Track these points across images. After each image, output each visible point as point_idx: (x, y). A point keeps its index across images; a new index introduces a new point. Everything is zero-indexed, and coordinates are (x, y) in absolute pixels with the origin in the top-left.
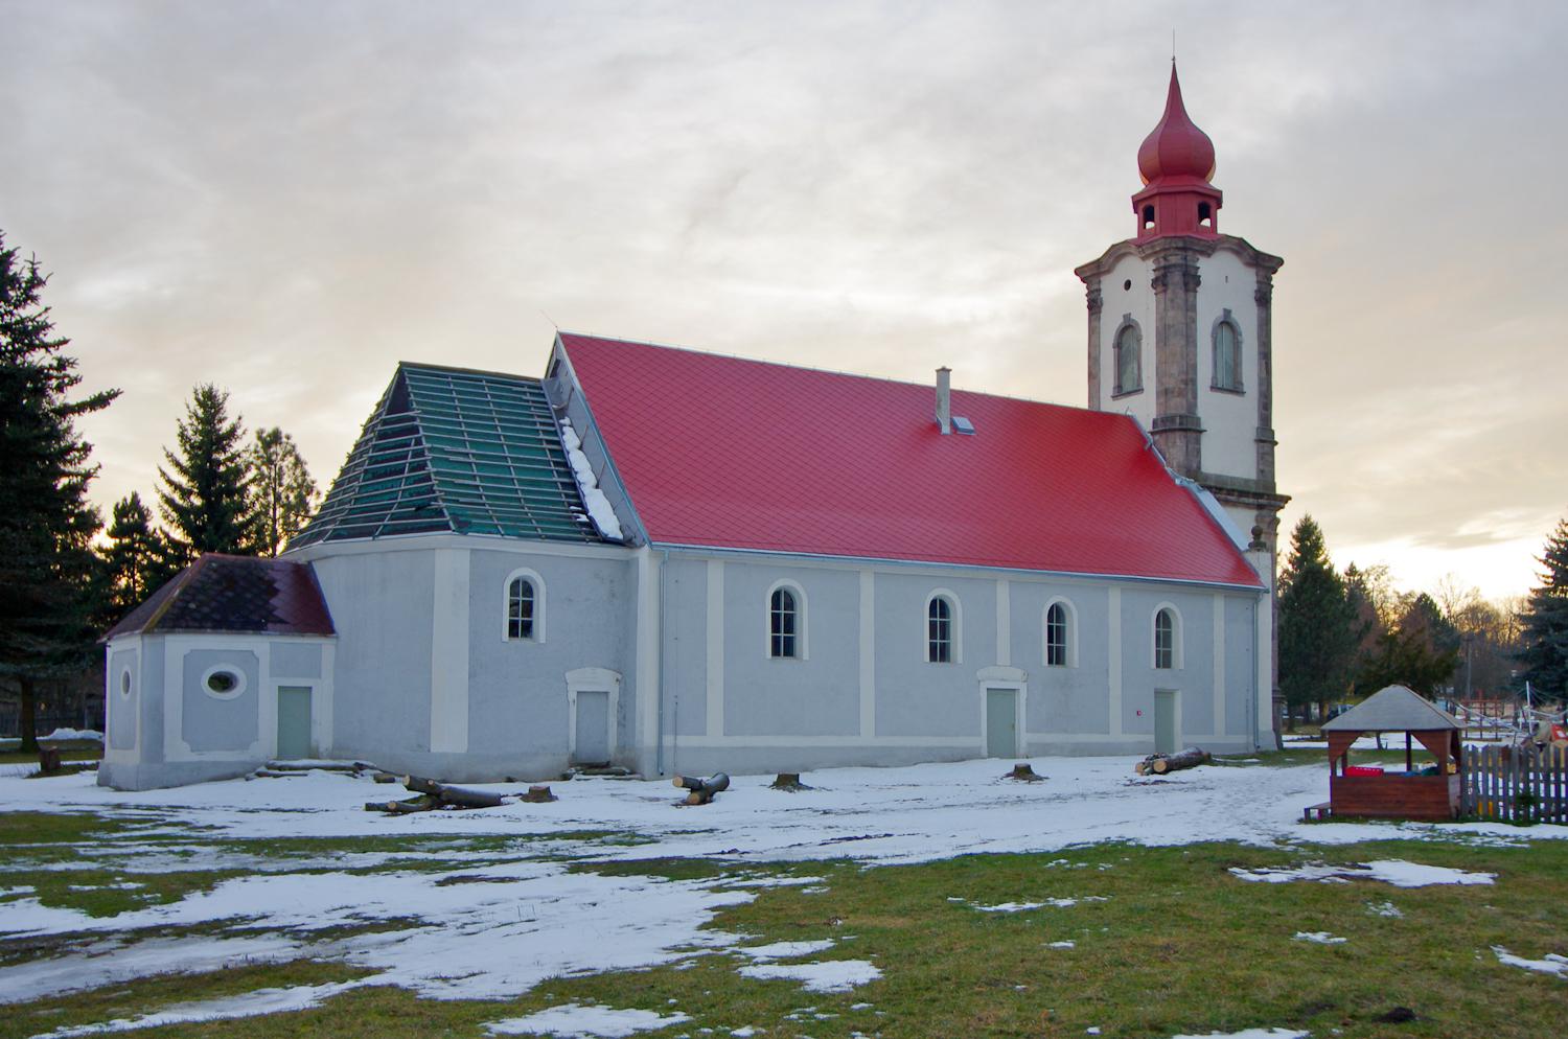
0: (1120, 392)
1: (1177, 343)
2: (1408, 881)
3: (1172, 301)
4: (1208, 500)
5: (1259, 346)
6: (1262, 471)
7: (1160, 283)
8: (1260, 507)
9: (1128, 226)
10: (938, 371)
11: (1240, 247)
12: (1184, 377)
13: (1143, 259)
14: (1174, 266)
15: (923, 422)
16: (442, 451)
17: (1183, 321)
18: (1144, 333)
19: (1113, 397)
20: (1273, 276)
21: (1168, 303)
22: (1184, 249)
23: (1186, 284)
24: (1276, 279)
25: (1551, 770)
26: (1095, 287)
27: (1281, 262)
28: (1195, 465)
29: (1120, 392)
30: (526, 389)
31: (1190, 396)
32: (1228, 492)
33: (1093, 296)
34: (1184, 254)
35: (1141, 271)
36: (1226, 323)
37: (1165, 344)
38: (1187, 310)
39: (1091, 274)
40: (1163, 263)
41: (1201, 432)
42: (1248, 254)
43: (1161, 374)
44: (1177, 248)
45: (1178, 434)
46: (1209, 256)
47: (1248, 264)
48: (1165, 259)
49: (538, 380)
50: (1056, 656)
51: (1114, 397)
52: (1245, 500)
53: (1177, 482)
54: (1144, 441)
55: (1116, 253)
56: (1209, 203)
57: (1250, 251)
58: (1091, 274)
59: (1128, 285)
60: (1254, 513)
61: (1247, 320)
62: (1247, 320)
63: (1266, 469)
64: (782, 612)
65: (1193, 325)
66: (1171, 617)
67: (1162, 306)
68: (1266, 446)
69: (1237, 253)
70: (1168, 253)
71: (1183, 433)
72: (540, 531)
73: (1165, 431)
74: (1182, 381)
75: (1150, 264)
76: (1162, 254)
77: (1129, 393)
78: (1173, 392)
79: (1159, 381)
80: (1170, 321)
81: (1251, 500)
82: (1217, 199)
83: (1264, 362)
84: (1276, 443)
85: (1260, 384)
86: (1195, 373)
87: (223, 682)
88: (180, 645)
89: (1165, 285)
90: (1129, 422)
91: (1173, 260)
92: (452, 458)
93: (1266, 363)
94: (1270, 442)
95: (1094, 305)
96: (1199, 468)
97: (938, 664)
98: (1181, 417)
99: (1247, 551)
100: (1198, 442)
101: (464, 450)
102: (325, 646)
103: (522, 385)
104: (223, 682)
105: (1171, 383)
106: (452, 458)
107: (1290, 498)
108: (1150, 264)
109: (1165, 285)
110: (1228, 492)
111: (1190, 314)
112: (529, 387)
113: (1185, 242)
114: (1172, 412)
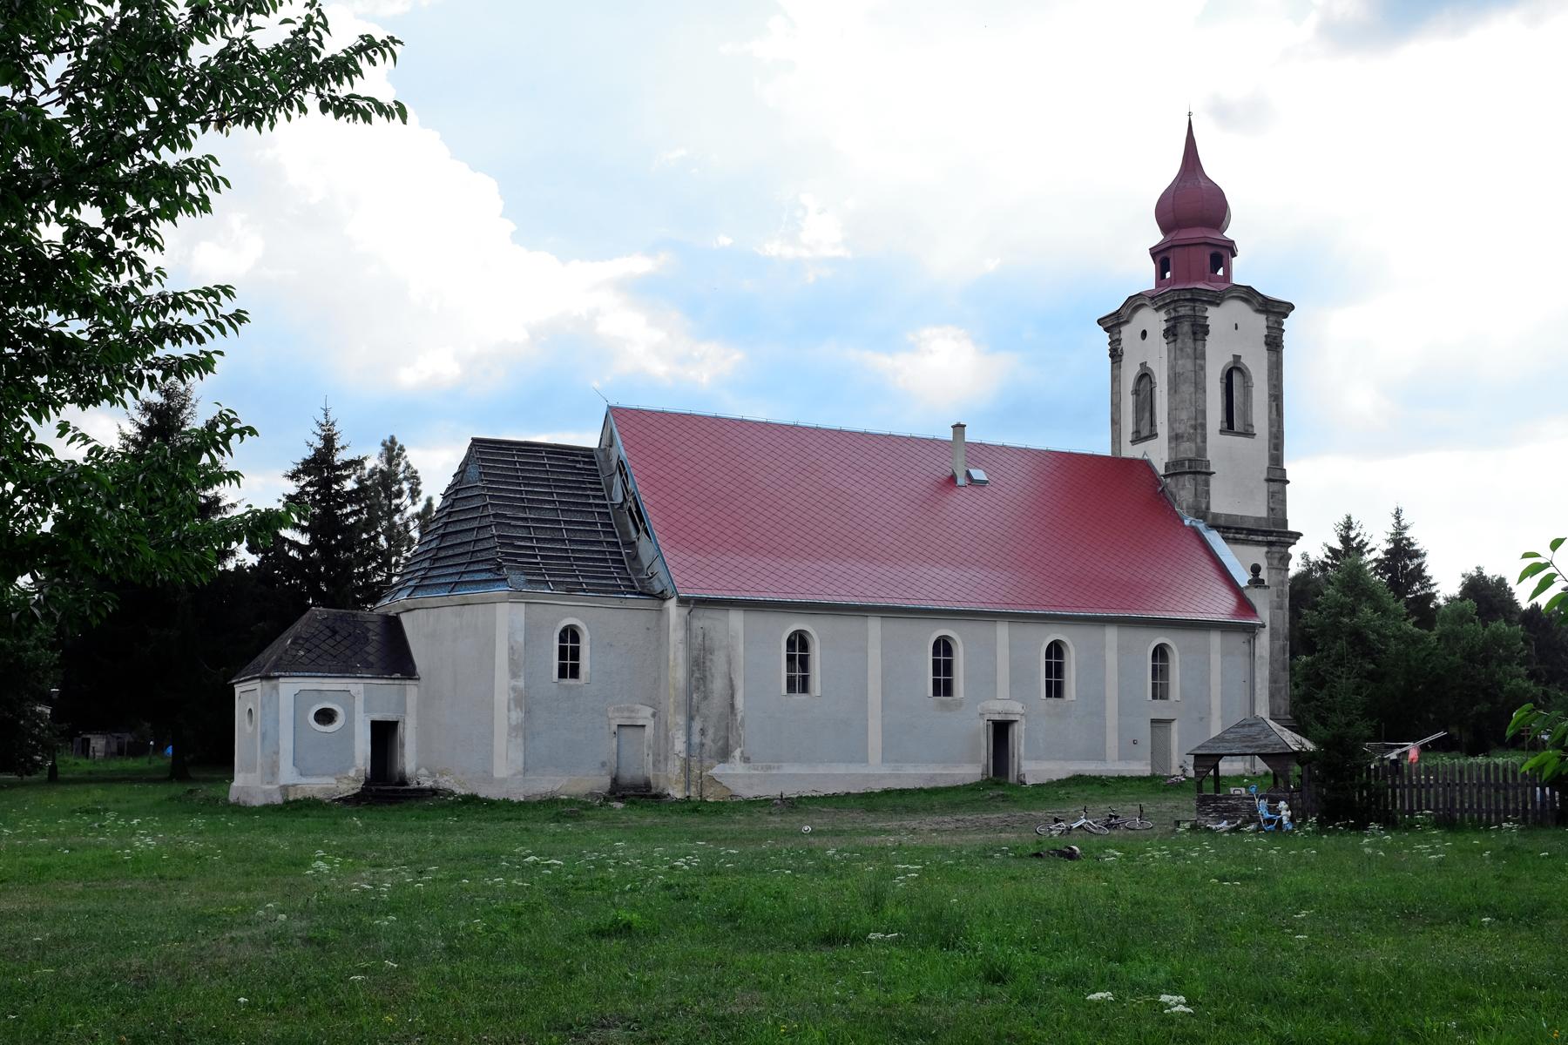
0: (1138, 438)
1: (1187, 389)
2: (366, 759)
4: (1215, 539)
6: (1273, 509)
7: (1171, 333)
8: (1270, 544)
9: (1144, 277)
11: (1248, 295)
12: (1193, 422)
13: (1157, 310)
14: (1184, 316)
15: (939, 475)
16: (505, 516)
21: (1178, 352)
22: (1192, 300)
23: (1194, 333)
26: (1116, 337)
27: (1291, 307)
28: (1204, 506)
29: (1138, 438)
30: (580, 458)
31: (1199, 440)
32: (1236, 532)
35: (1153, 321)
36: (1234, 373)
38: (1196, 358)
39: (1113, 323)
40: (1173, 315)
42: (1258, 302)
43: (1172, 421)
45: (1187, 477)
47: (1257, 311)
49: (591, 450)
50: (1055, 689)
51: (1133, 442)
53: (1187, 522)
54: (1159, 483)
55: (1134, 304)
56: (1223, 253)
57: (1260, 299)
58: (1113, 323)
59: (1144, 334)
60: (1265, 549)
64: (797, 653)
65: (1202, 373)
66: (1064, 648)
67: (1172, 356)
68: (1276, 486)
72: (585, 586)
74: (1191, 426)
75: (1162, 315)
77: (1146, 438)
78: (1182, 437)
81: (1260, 538)
82: (1230, 248)
83: (1274, 404)
84: (1288, 482)
85: (1271, 426)
86: (1204, 418)
87: (325, 716)
88: (289, 687)
89: (1175, 335)
90: (1145, 465)
91: (1183, 311)
92: (513, 523)
93: (1277, 405)
94: (1280, 481)
95: (1116, 355)
96: (1208, 508)
97: (1052, 700)
98: (1190, 460)
99: (1247, 587)
100: (1207, 484)
101: (525, 516)
102: (412, 690)
103: (577, 455)
104: (325, 716)
106: (513, 523)
108: (1162, 315)
109: (1175, 335)
110: (1236, 532)
111: (1198, 362)
112: (547, 452)
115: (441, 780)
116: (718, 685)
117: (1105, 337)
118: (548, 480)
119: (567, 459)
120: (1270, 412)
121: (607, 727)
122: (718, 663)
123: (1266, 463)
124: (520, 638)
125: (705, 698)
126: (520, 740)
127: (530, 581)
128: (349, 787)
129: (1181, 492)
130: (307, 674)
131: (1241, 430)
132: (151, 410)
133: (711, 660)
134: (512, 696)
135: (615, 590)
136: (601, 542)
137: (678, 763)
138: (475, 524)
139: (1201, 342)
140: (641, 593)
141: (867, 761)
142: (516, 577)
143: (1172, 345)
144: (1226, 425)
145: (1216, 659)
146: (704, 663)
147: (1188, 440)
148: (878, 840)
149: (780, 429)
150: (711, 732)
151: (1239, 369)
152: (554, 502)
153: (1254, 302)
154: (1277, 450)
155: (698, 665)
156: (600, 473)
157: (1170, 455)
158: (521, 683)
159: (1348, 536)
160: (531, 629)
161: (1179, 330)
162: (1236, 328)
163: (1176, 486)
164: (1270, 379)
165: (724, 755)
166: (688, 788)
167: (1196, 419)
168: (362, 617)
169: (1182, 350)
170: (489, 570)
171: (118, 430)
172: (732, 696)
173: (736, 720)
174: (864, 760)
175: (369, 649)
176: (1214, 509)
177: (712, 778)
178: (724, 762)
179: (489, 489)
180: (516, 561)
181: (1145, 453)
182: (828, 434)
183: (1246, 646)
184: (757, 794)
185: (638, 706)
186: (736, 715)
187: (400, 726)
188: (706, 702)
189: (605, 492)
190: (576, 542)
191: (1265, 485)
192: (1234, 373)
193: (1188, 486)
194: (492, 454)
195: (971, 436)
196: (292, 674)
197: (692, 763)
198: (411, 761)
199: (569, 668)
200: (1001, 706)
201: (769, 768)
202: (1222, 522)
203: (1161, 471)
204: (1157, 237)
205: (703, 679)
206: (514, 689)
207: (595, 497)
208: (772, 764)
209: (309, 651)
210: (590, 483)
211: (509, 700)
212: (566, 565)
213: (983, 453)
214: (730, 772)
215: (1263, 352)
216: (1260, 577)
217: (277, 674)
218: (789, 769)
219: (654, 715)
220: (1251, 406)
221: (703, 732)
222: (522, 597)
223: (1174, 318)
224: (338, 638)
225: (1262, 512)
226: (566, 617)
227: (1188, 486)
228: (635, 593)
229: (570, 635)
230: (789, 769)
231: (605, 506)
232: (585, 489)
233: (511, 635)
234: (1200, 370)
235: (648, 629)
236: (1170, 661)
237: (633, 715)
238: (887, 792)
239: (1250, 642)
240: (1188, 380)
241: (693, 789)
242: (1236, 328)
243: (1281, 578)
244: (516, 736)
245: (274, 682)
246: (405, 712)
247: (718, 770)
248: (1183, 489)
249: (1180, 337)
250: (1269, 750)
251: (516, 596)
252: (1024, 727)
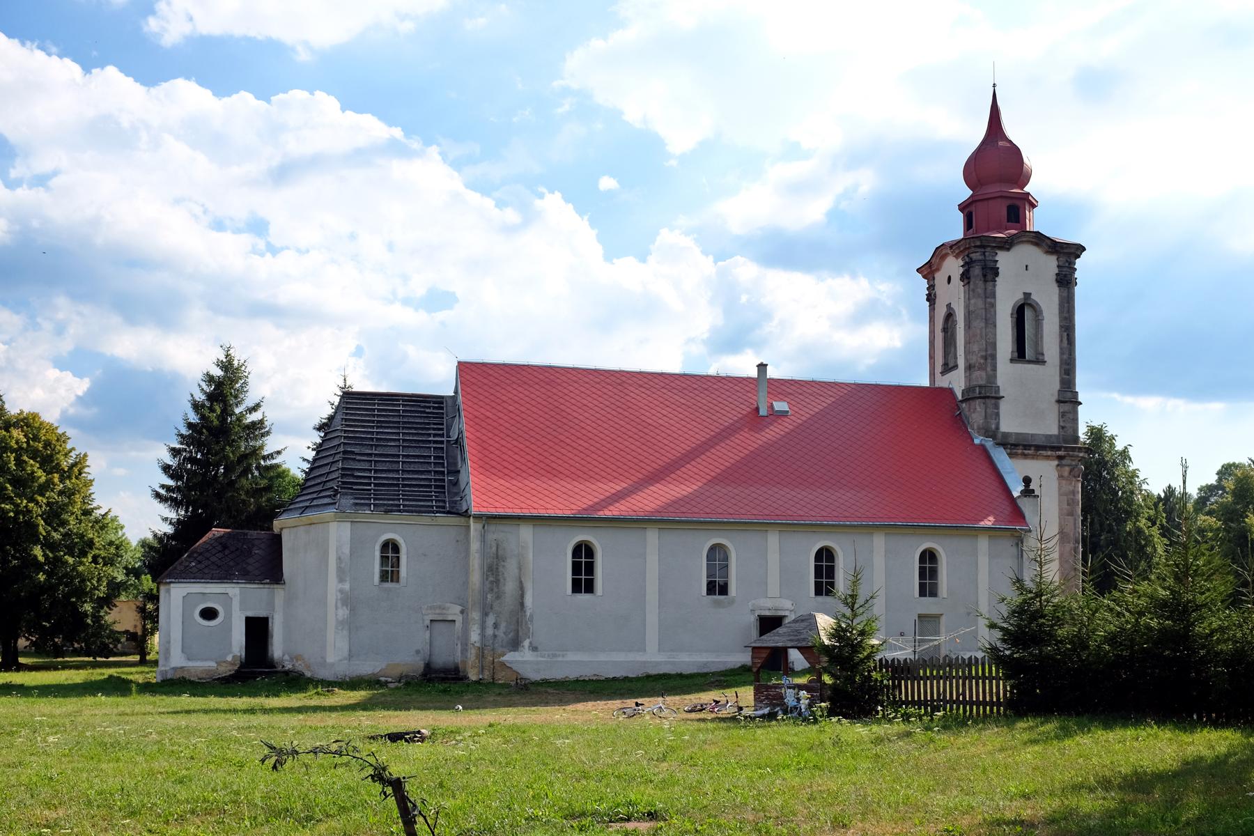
1: (978, 324)
5: (1060, 321)
6: (1063, 428)
10: (758, 366)
11: (1039, 240)
12: (984, 354)
16: (353, 453)
17: (983, 306)
23: (985, 276)
25: (980, 678)
26: (932, 283)
28: (993, 426)
30: (432, 405)
31: (989, 369)
34: (983, 250)
37: (969, 327)
39: (928, 271)
42: (1047, 244)
43: (967, 352)
44: (975, 247)
45: (978, 401)
46: (1008, 249)
47: (1047, 252)
48: (968, 256)
51: (943, 373)
52: (1044, 453)
53: (977, 441)
57: (1049, 242)
60: (1056, 463)
61: (1048, 300)
62: (1048, 300)
63: (1068, 425)
65: (992, 310)
68: (1066, 407)
69: (1037, 244)
70: (971, 251)
71: (983, 401)
74: (982, 357)
76: (966, 253)
78: (974, 367)
79: (966, 359)
81: (1049, 453)
83: (1065, 334)
84: (1081, 403)
85: (1062, 353)
87: (209, 614)
90: (950, 391)
93: (1068, 335)
95: (931, 298)
96: (998, 428)
98: (980, 387)
99: (1019, 497)
100: (997, 407)
101: (370, 452)
102: (279, 593)
103: (429, 402)
104: (209, 614)
109: (969, 278)
111: (988, 300)
112: (434, 403)
113: (981, 241)
115: (297, 664)
116: (510, 587)
117: (924, 283)
118: (399, 422)
119: (419, 406)
120: (1061, 341)
121: (421, 622)
122: (510, 569)
123: (1056, 386)
124: (347, 550)
125: (498, 597)
126: (345, 633)
127: (356, 504)
128: (225, 670)
129: (973, 415)
130: (192, 580)
131: (1034, 359)
132: (214, 382)
133: (504, 566)
134: (339, 597)
135: (429, 510)
136: (430, 472)
137: (473, 651)
139: (991, 283)
140: (449, 512)
141: (645, 650)
142: (347, 501)
143: (967, 286)
144: (1016, 354)
145: (983, 561)
146: (497, 569)
147: (979, 369)
149: (616, 375)
150: (503, 626)
151: (1030, 305)
152: (399, 440)
154: (1068, 375)
155: (492, 570)
156: (445, 416)
157: (965, 383)
158: (347, 586)
159: (10, 427)
160: (357, 545)
161: (971, 273)
162: (1027, 266)
163: (969, 411)
164: (1061, 312)
165: (515, 645)
166: (482, 669)
167: (986, 351)
168: (251, 535)
169: (973, 291)
170: (329, 496)
171: (190, 398)
172: (522, 596)
173: (525, 616)
174: (643, 649)
175: (251, 560)
176: (1004, 428)
177: (503, 664)
178: (514, 651)
179: (345, 431)
180: (351, 489)
181: (950, 383)
182: (723, 381)
183: (1014, 550)
184: (543, 677)
185: (448, 605)
186: (525, 612)
187: (270, 620)
188: (498, 602)
189: (445, 432)
190: (408, 472)
191: (1056, 406)
194: (356, 403)
195: (772, 373)
196: (180, 580)
197: (486, 652)
198: (278, 648)
199: (390, 574)
200: (769, 605)
201: (555, 656)
202: (1012, 440)
203: (960, 397)
204: (967, 193)
205: (497, 582)
206: (341, 591)
207: (435, 435)
208: (558, 653)
209: (200, 562)
210: (434, 424)
211: (337, 600)
212: (395, 491)
213: (782, 387)
214: (520, 659)
215: (1055, 289)
216: (1031, 487)
217: (168, 580)
218: (572, 657)
219: (462, 612)
220: (1042, 337)
221: (496, 626)
222: (347, 517)
224: (227, 552)
225: (1053, 430)
226: (386, 533)
227: (978, 409)
228: (444, 513)
229: (390, 548)
230: (572, 657)
231: (442, 442)
232: (429, 429)
233: (338, 548)
234: (990, 307)
235: (458, 541)
236: (939, 563)
237: (444, 611)
238: (577, 681)
239: (1017, 544)
240: (983, 315)
241: (486, 673)
242: (1027, 266)
243: (1071, 488)
244: (342, 629)
246: (273, 610)
247: (509, 657)
248: (974, 412)
249: (972, 280)
250: (804, 644)
251: (342, 515)
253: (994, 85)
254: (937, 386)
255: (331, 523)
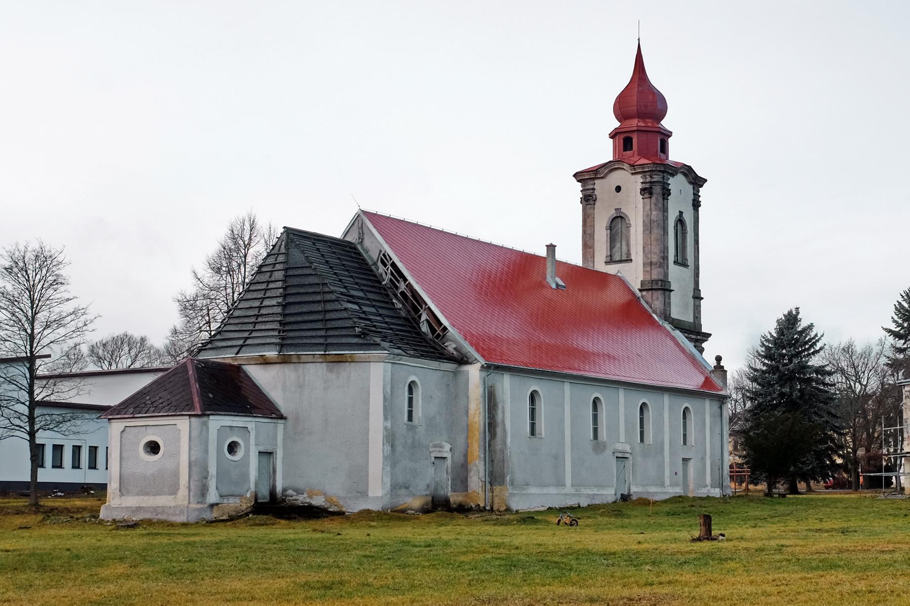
0: (611, 261)
1: (657, 232)
3: (656, 205)
7: (647, 191)
12: (663, 255)
14: (657, 182)
18: (632, 222)
19: (606, 263)
20: (700, 189)
22: (663, 172)
24: (702, 191)
33: (589, 192)
36: (680, 221)
39: (587, 177)
40: (648, 180)
41: (671, 291)
45: (660, 292)
47: (690, 183)
59: (618, 189)
61: (688, 218)
67: (648, 207)
69: (685, 175)
73: (652, 289)
74: (661, 257)
80: (653, 218)
95: (588, 199)
96: (670, 314)
105: (655, 258)
107: (710, 335)
108: (639, 179)
114: (654, 277)
138: (318, 298)
148: (192, 539)
153: (690, 176)
192: (680, 221)
193: (660, 298)
215: (691, 208)
223: (651, 182)
234: (665, 219)
245: (205, 419)
246: (276, 445)
252: (631, 462)
253: (639, 40)
254: (595, 269)
255: (371, 363)
